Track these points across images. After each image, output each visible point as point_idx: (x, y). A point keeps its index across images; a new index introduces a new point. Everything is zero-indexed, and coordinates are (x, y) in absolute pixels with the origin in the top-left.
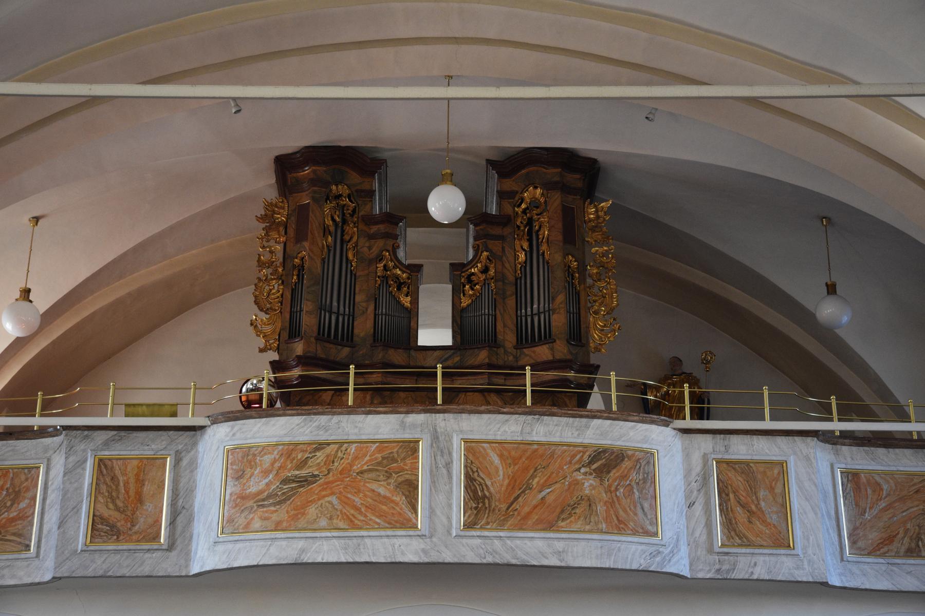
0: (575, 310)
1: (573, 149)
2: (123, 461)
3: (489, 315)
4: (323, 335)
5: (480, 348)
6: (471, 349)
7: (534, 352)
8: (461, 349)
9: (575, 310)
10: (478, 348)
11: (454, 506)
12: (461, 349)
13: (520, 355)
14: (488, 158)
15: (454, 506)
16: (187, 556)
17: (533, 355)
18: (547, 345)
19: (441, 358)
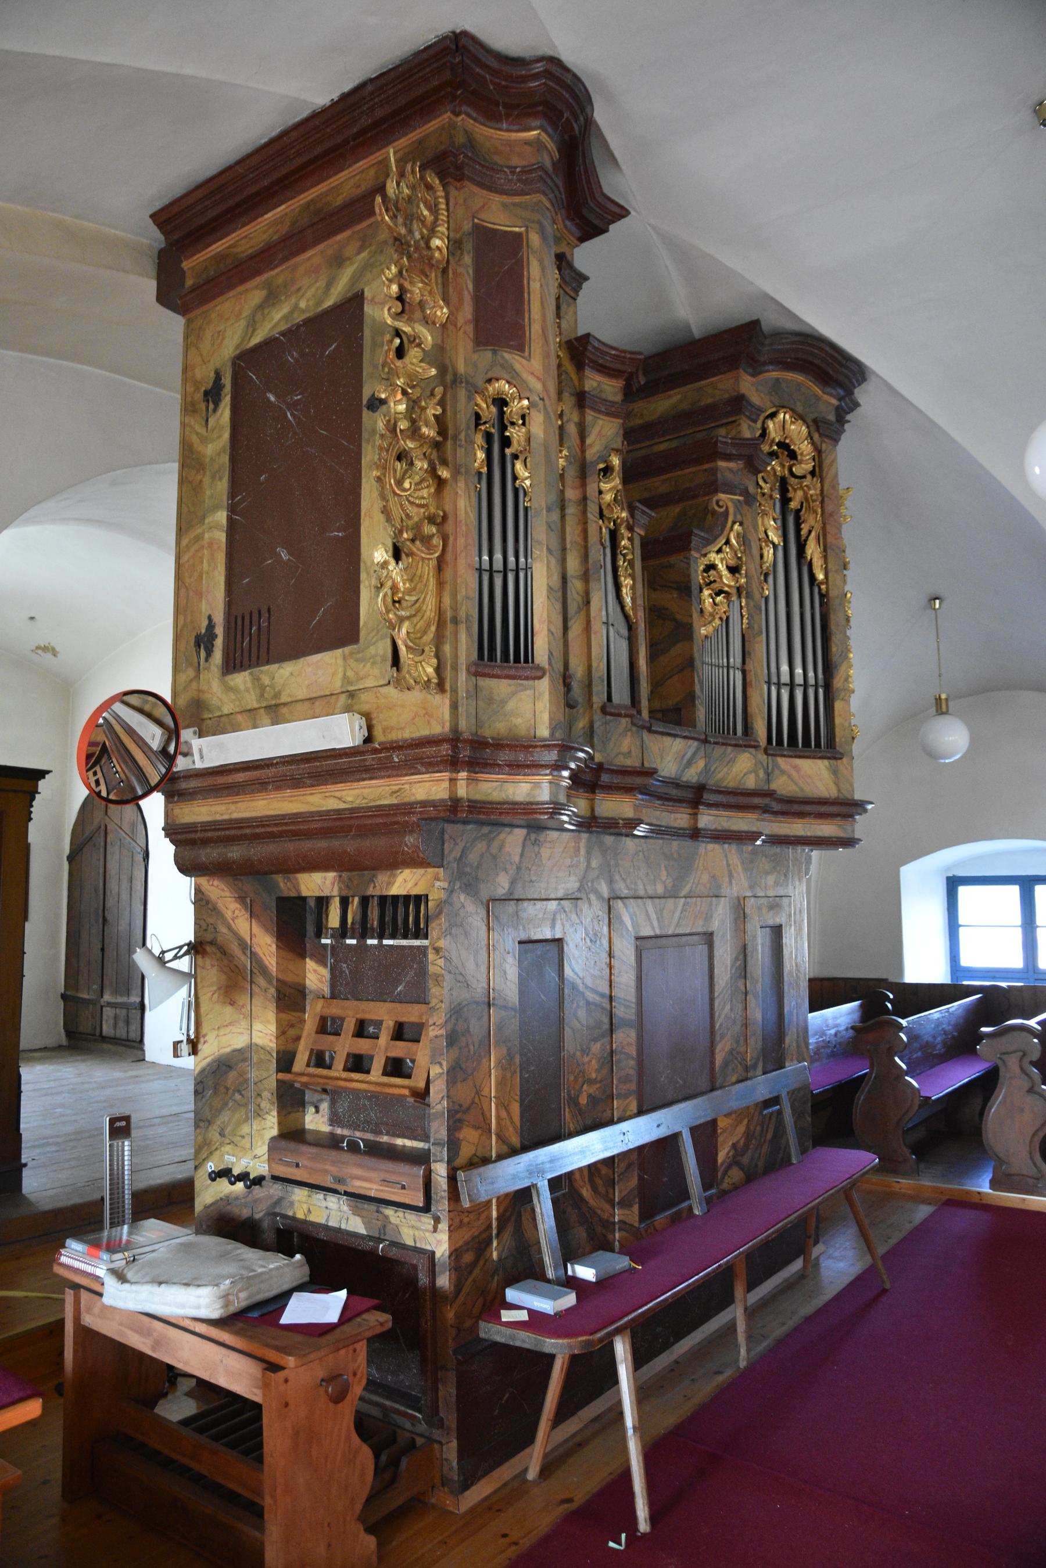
0: (811, 674)
1: (866, 366)
2: (559, 904)
3: (792, 685)
4: (735, 733)
5: (741, 746)
6: (723, 744)
7: (797, 768)
8: (710, 742)
9: (811, 674)
10: (736, 745)
11: (946, 1186)
12: (710, 742)
13: (773, 769)
14: (151, 212)
15: (946, 1186)
16: (272, 1048)
17: (794, 773)
18: (826, 762)
19: (684, 756)
